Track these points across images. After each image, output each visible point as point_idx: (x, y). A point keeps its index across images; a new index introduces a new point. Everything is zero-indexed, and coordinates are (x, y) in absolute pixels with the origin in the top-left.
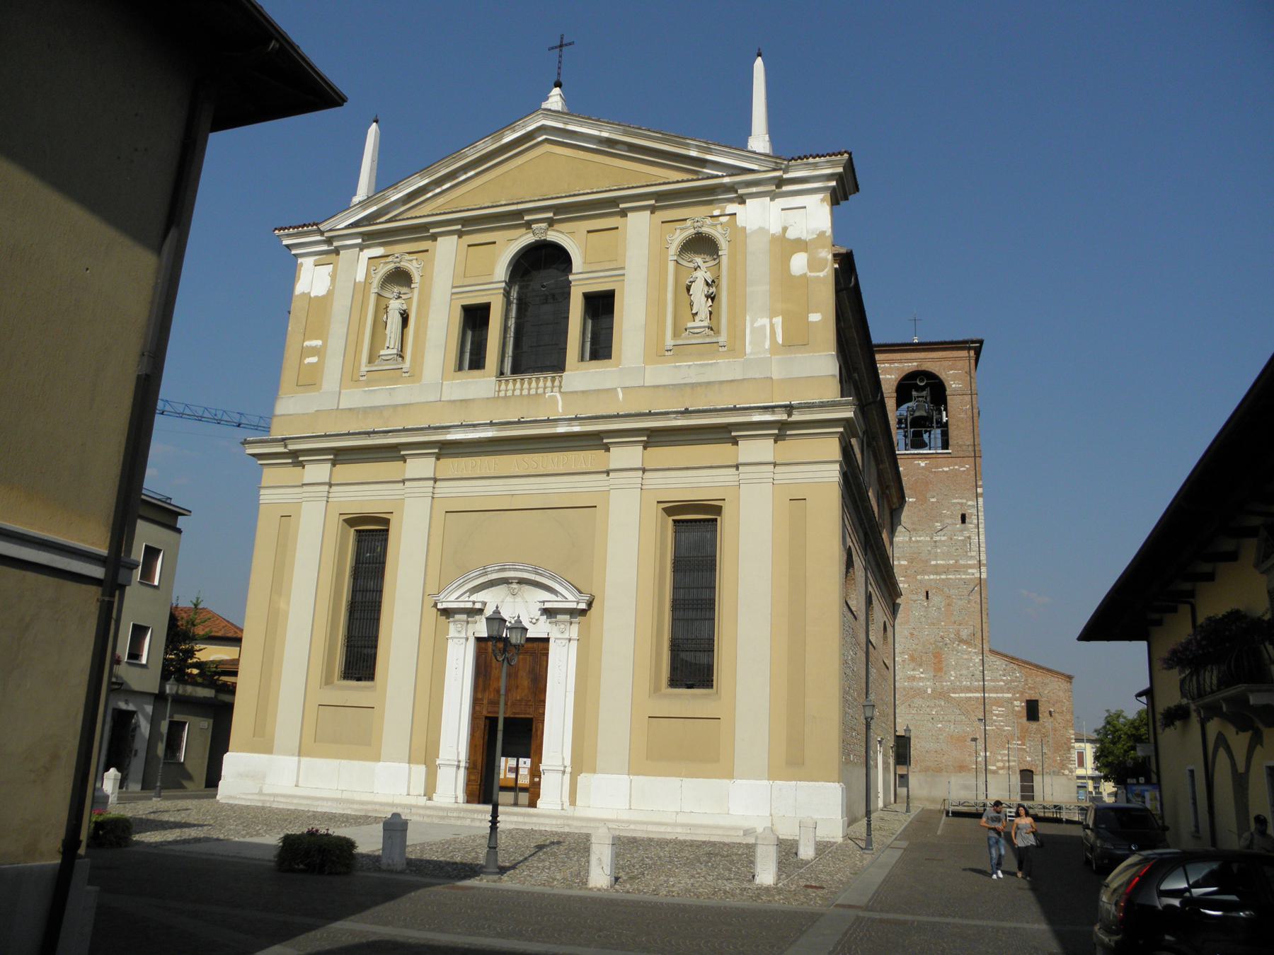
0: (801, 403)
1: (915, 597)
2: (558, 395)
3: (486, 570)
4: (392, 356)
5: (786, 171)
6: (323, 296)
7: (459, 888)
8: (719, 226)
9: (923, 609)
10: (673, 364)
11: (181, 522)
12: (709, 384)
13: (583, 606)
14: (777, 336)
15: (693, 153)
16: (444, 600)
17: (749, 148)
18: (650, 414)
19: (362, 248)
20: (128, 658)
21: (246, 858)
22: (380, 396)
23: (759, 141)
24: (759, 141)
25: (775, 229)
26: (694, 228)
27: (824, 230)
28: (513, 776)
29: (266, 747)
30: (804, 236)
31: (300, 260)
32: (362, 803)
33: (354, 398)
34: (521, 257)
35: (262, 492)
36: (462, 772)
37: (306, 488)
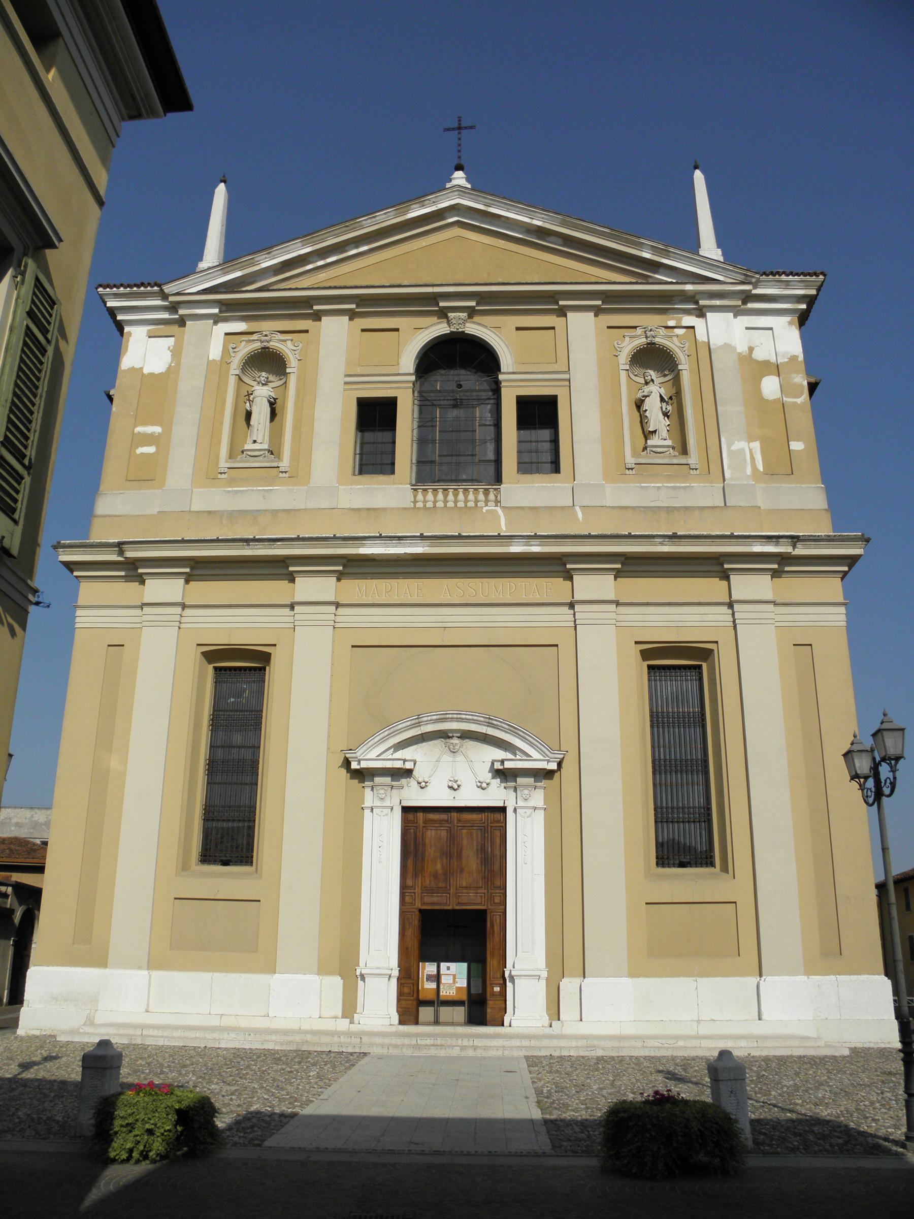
0: (805, 536)
3: (420, 720)
4: (262, 453)
6: (161, 374)
8: (675, 339)
12: (687, 508)
13: (553, 766)
14: (756, 462)
15: (647, 255)
19: (217, 320)
21: (391, 1152)
25: (742, 348)
26: (647, 337)
28: (433, 986)
32: (285, 1032)
35: (79, 612)
36: (394, 982)
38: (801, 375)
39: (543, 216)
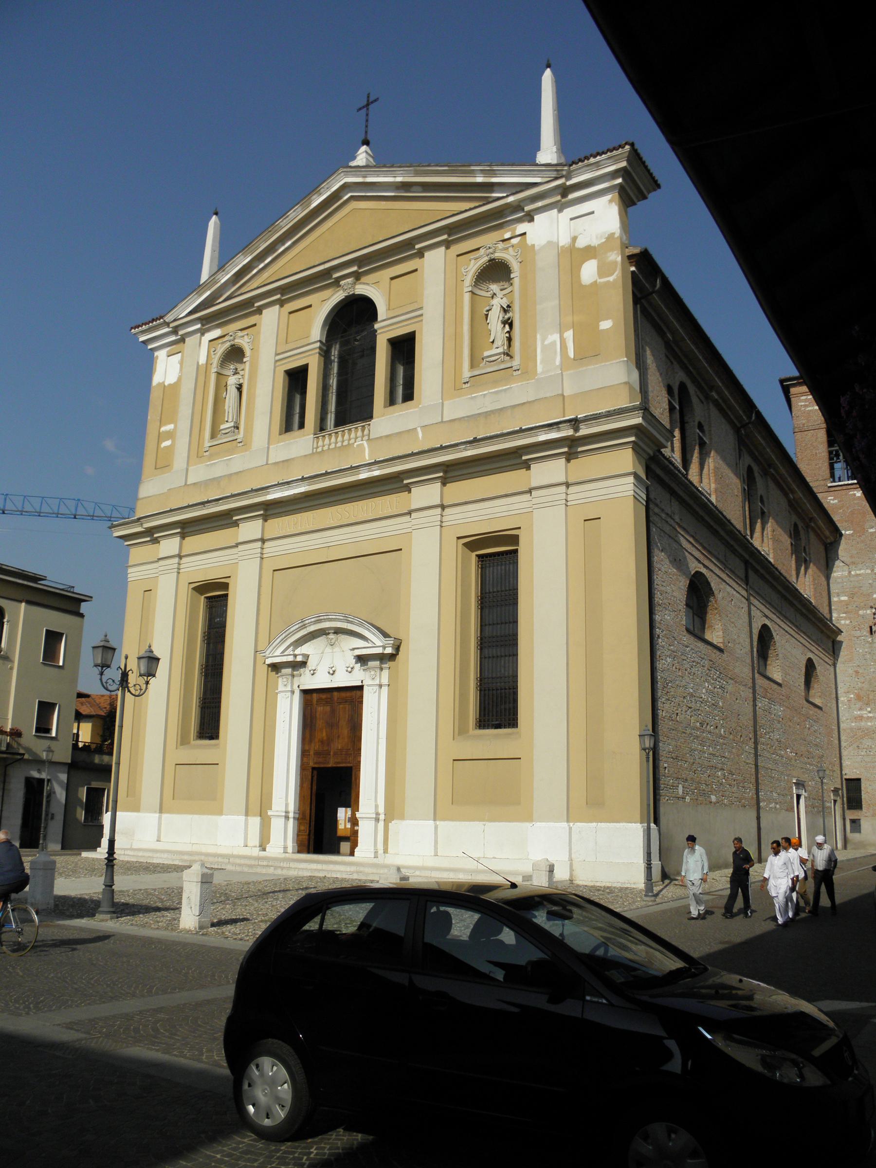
1: (858, 633)
2: (365, 443)
5: (568, 177)
7: (59, 926)
8: (511, 249)
9: (867, 645)
10: (470, 396)
11: (84, 608)
13: (389, 650)
14: (568, 350)
15: (480, 179)
16: (270, 655)
17: (537, 162)
18: (442, 448)
19: (202, 332)
20: (36, 732)
22: (219, 468)
23: (548, 153)
24: (548, 153)
25: (564, 240)
27: (613, 232)
29: (136, 808)
30: (595, 242)
31: (156, 354)
33: (199, 473)
34: (335, 315)
35: (130, 570)
37: (161, 563)
38: (615, 252)
39: (401, 172)
